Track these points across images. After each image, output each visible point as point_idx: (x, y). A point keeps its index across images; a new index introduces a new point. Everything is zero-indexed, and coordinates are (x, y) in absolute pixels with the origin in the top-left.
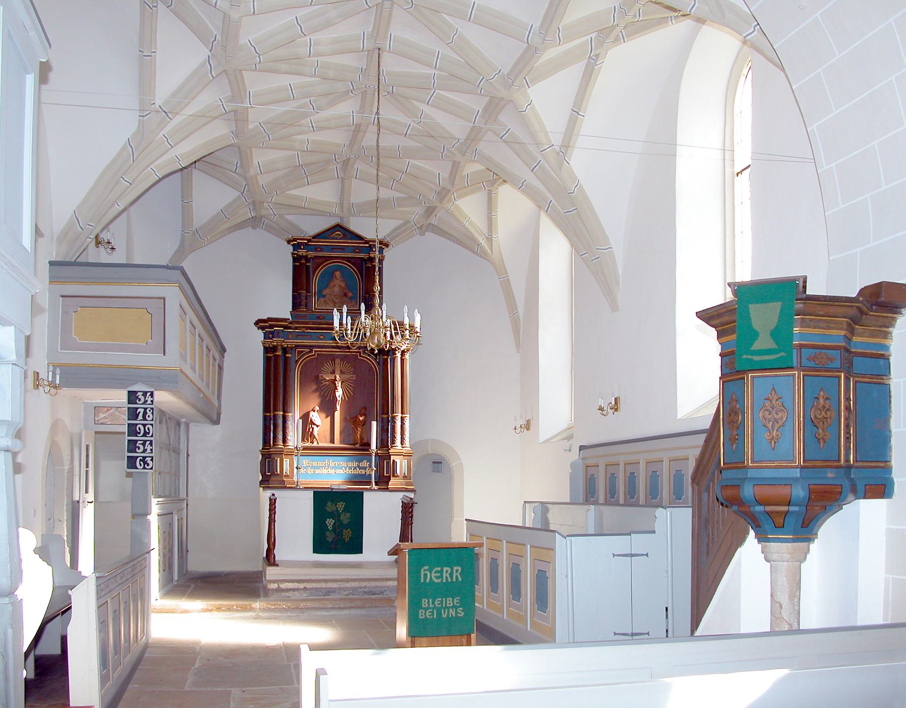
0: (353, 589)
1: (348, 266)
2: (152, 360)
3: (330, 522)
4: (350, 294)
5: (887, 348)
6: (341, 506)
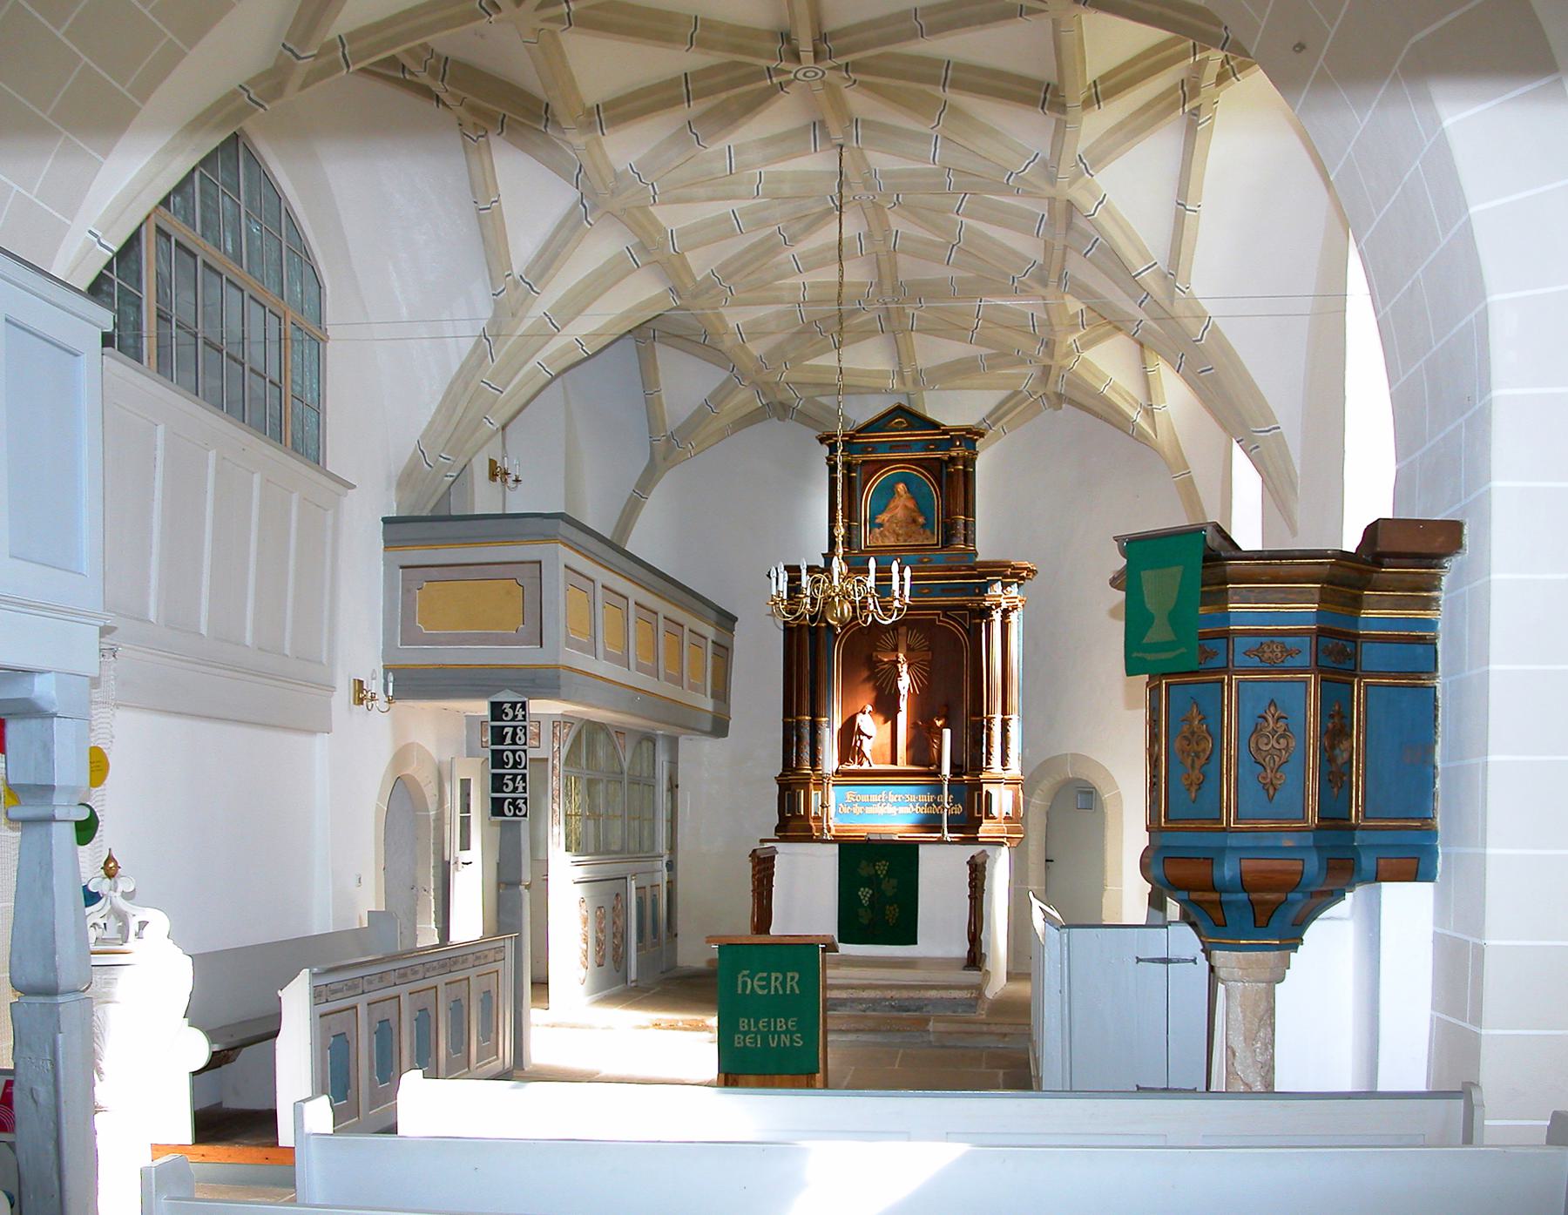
0: (874, 1001)
1: (917, 473)
2: (524, 655)
3: (865, 894)
4: (921, 520)
5: (1431, 625)
6: (882, 867)
